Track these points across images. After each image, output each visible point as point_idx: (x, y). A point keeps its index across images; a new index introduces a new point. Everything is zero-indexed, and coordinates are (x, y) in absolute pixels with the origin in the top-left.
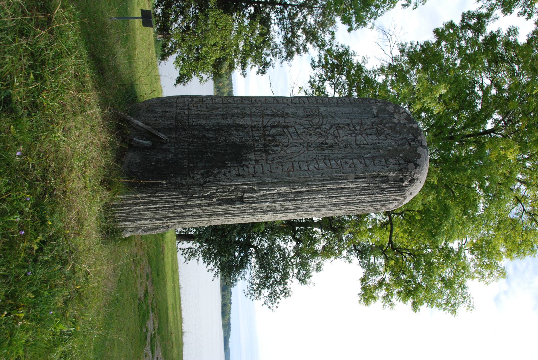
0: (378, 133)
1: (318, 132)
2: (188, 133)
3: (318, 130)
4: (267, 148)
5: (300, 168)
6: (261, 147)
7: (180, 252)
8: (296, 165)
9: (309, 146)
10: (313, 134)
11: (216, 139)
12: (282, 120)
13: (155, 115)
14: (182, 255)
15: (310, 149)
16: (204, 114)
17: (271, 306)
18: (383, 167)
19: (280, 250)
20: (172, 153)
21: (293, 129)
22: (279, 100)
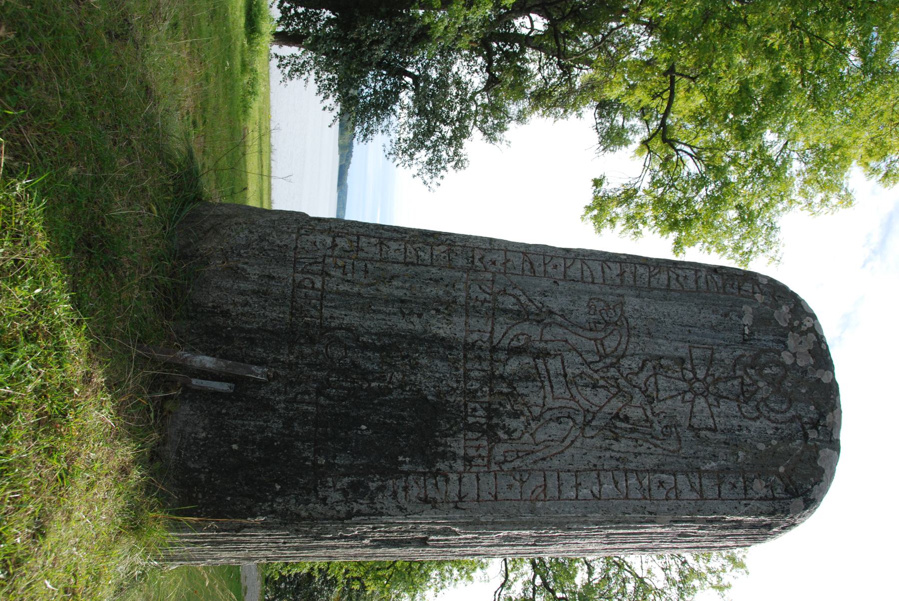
0: (745, 395)
1: (613, 377)
2: (318, 353)
3: (613, 372)
4: (495, 421)
5: (560, 492)
6: (480, 416)
7: (275, 62)
8: (552, 483)
9: (587, 423)
10: (602, 382)
11: (381, 378)
12: (535, 331)
13: (243, 285)
14: (279, 67)
15: (589, 432)
16: (359, 294)
17: (429, 181)
18: (736, 503)
19: (458, 83)
20: (280, 417)
21: (558, 364)
22: (538, 261)
